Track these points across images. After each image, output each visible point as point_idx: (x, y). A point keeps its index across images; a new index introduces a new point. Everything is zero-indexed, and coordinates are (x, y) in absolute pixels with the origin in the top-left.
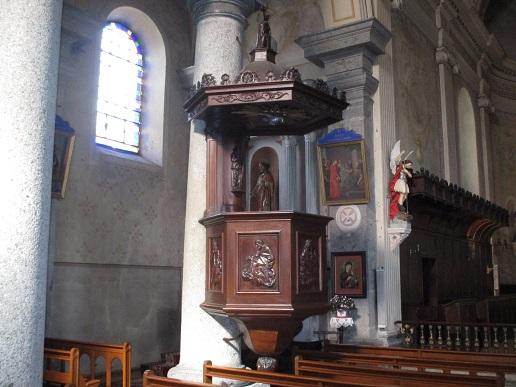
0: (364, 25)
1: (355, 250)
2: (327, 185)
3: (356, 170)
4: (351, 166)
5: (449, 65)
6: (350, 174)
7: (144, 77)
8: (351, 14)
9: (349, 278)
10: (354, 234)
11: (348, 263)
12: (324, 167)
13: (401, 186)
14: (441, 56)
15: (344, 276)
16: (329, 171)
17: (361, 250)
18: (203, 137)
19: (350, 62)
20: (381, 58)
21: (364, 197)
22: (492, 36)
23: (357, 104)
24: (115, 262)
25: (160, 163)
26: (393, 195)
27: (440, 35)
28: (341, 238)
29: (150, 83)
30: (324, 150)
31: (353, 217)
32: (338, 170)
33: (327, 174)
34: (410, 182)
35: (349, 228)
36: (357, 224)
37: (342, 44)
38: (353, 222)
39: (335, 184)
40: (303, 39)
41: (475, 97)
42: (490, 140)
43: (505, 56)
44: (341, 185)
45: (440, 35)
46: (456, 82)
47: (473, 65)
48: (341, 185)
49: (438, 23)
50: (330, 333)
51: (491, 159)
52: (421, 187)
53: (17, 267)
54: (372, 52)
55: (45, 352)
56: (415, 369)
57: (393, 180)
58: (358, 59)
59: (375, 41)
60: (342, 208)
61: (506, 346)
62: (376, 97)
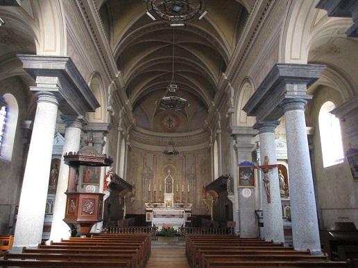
0: (65, 59)
2: (84, 177)
5: (122, 132)
7: (6, 121)
8: (53, 49)
13: (109, 180)
14: (120, 129)
18: (68, 166)
20: (108, 134)
22: (119, 72)
25: (10, 160)
26: (105, 182)
27: (121, 120)
29: (8, 124)
34: (111, 178)
37: (96, 129)
41: (126, 142)
42: (129, 157)
43: (137, 126)
45: (121, 120)
46: (122, 136)
47: (126, 128)
49: (120, 116)
52: (114, 180)
54: (105, 133)
55: (282, 201)
56: (20, 260)
57: (106, 177)
58: (101, 134)
59: (67, 70)
60: (88, 186)
62: (104, 148)
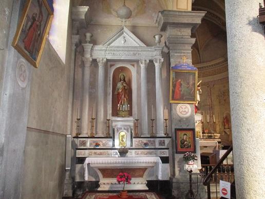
1: (188, 128)
3: (191, 86)
4: (188, 84)
6: (188, 87)
9: (185, 143)
10: (187, 119)
11: (185, 134)
12: (173, 82)
15: (183, 142)
16: (176, 84)
17: (191, 128)
19: (183, 31)
21: (194, 101)
23: (188, 53)
24: (56, 174)
28: (180, 121)
30: (174, 73)
31: (187, 110)
32: (181, 85)
33: (174, 86)
35: (185, 116)
36: (189, 114)
38: (187, 113)
39: (178, 92)
40: (165, 12)
44: (182, 93)
48: (182, 93)
50: (173, 174)
51: (188, 101)
53: (258, 154)
60: (180, 105)
61: (230, 174)
